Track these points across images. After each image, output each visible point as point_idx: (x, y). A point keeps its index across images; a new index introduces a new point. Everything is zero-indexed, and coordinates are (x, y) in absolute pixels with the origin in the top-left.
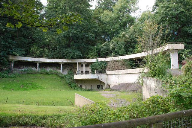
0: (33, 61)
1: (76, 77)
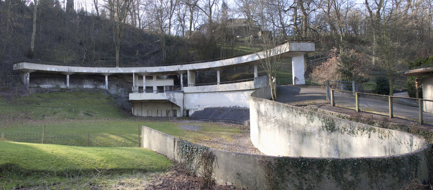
0: (60, 70)
1: (134, 96)
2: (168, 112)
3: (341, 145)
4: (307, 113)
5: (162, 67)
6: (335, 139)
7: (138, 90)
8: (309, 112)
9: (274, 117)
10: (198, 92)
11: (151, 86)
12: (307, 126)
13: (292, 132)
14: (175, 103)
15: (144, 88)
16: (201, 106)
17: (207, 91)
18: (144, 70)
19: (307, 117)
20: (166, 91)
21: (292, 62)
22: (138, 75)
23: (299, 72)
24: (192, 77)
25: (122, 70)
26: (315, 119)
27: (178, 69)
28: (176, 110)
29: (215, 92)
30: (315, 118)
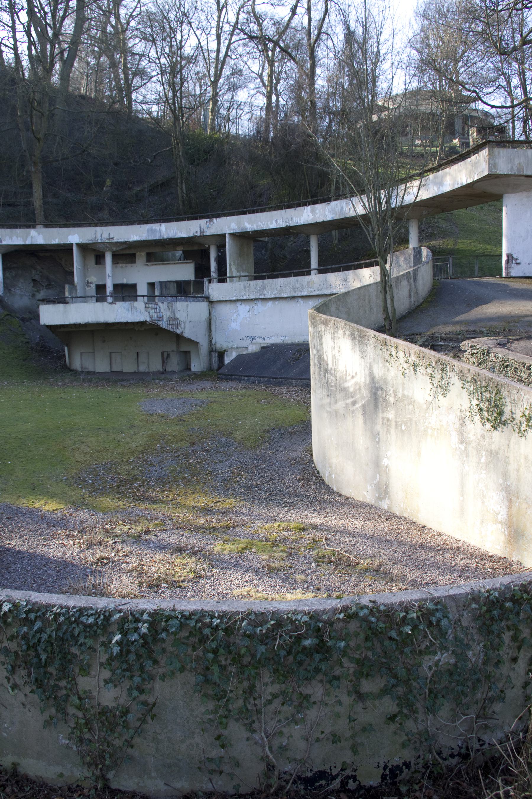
2: (165, 356)
3: (516, 472)
4: (433, 364)
5: (155, 226)
6: (501, 452)
7: (94, 294)
8: (436, 363)
9: (354, 375)
10: (248, 297)
11: (131, 281)
12: (431, 407)
13: (393, 424)
14: (178, 331)
15: (109, 289)
16: (257, 340)
17: (273, 296)
18: (106, 236)
19: (432, 377)
20: (161, 296)
21: (504, 209)
22: (94, 250)
23: (524, 240)
24: (241, 254)
25: (41, 236)
26: (451, 385)
27: (201, 232)
28: (189, 352)
29: (293, 298)
30: (452, 381)
